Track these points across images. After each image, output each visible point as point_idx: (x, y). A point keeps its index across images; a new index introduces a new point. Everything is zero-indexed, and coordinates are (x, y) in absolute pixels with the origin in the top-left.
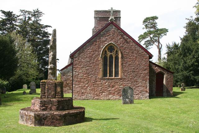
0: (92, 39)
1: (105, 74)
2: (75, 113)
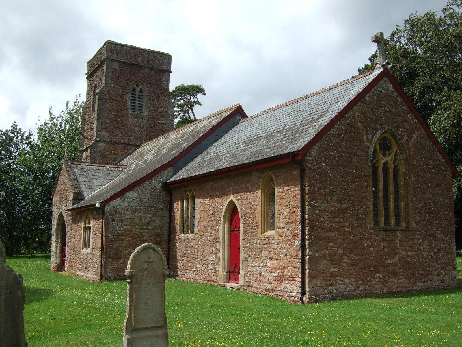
1: (376, 222)
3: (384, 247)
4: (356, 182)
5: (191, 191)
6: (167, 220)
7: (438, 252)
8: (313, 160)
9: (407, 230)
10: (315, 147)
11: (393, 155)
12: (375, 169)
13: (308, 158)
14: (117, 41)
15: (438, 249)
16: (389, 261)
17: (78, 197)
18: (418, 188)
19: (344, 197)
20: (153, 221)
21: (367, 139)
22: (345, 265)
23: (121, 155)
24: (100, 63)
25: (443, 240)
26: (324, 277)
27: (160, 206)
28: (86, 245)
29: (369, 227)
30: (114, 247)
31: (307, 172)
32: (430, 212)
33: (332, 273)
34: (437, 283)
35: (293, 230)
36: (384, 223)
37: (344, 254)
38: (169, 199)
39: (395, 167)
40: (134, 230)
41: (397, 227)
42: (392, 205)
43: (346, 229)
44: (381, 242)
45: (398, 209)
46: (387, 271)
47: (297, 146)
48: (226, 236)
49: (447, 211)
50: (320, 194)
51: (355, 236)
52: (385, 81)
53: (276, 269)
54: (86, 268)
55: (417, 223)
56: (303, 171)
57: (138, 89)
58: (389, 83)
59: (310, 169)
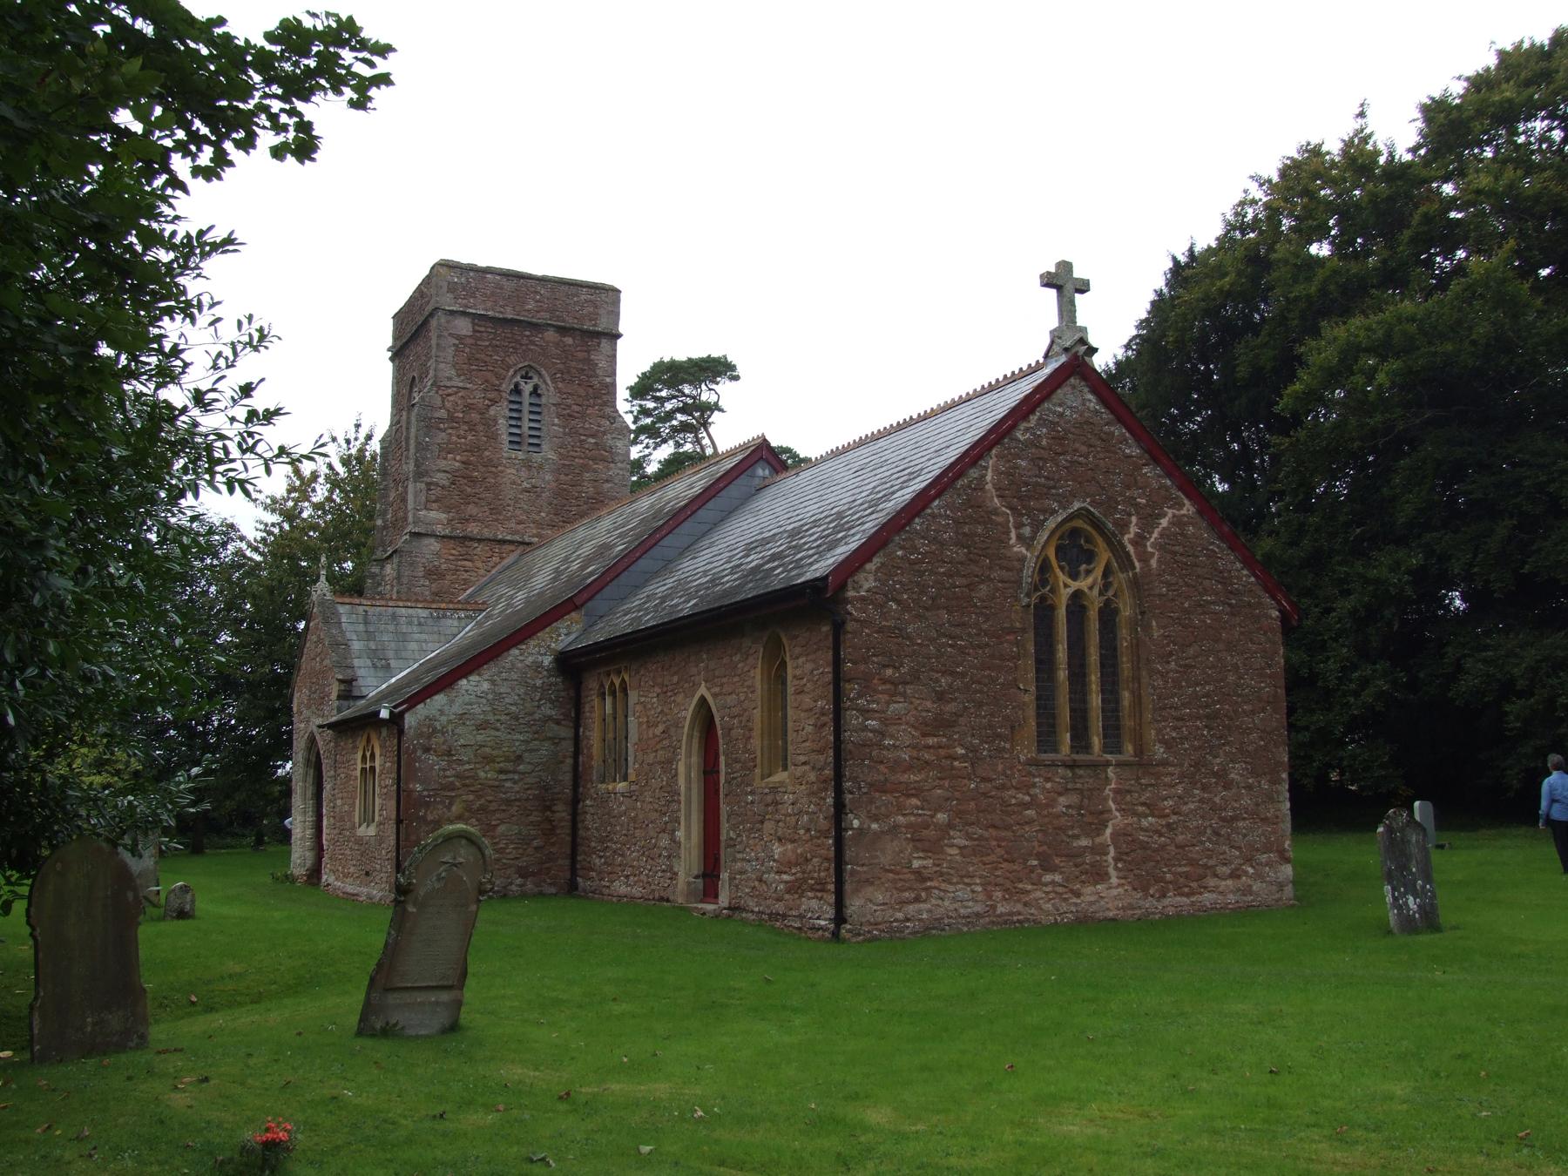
0: (960, 475)
1: (1047, 739)
2: (250, 559)
3: (1068, 807)
4: (987, 645)
5: (619, 672)
6: (568, 747)
7: (1234, 819)
8: (863, 599)
9: (1142, 763)
10: (870, 566)
11: (1098, 572)
12: (1044, 612)
13: (851, 594)
14: (464, 258)
15: (1234, 809)
16: (1084, 842)
17: (348, 691)
18: (1171, 654)
19: (950, 686)
20: (531, 751)
21: (1020, 537)
22: (954, 851)
23: (482, 572)
24: (420, 319)
25: (1249, 787)
26: (894, 881)
27: (548, 710)
28: (367, 819)
29: (1022, 758)
30: (430, 818)
31: (850, 626)
32: (1208, 717)
33: (917, 872)
34: (1232, 898)
35: (822, 769)
36: (1072, 747)
37: (950, 826)
38: (572, 693)
39: (1108, 602)
40: (482, 774)
41: (1109, 757)
42: (1096, 700)
43: (956, 763)
44: (1060, 794)
45: (1116, 710)
46: (1076, 866)
47: (820, 567)
48: (695, 787)
49: (1263, 710)
50: (884, 681)
51: (984, 779)
52: (1074, 387)
53: (790, 864)
54: (367, 874)
55: (1168, 745)
56: (838, 628)
57: (527, 388)
58: (1086, 390)
59: (857, 620)
